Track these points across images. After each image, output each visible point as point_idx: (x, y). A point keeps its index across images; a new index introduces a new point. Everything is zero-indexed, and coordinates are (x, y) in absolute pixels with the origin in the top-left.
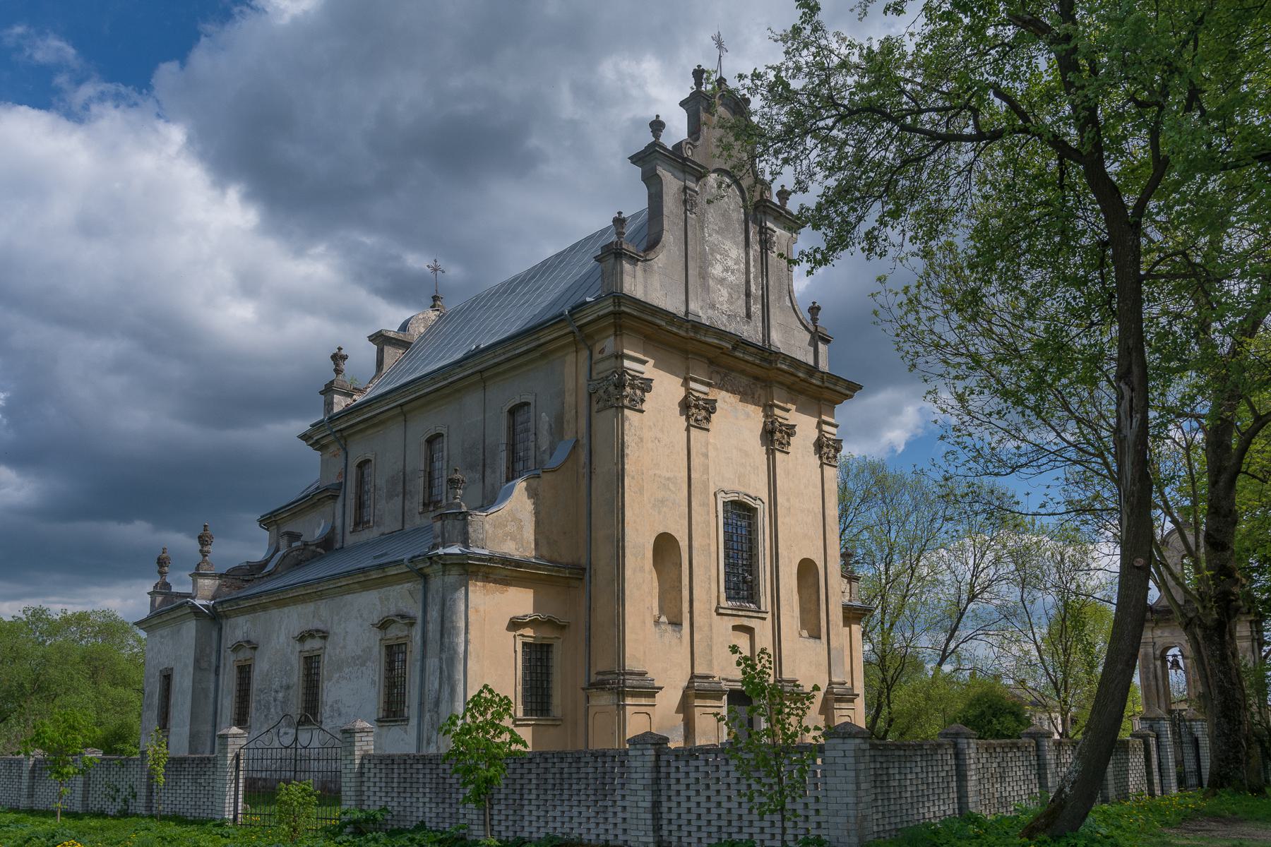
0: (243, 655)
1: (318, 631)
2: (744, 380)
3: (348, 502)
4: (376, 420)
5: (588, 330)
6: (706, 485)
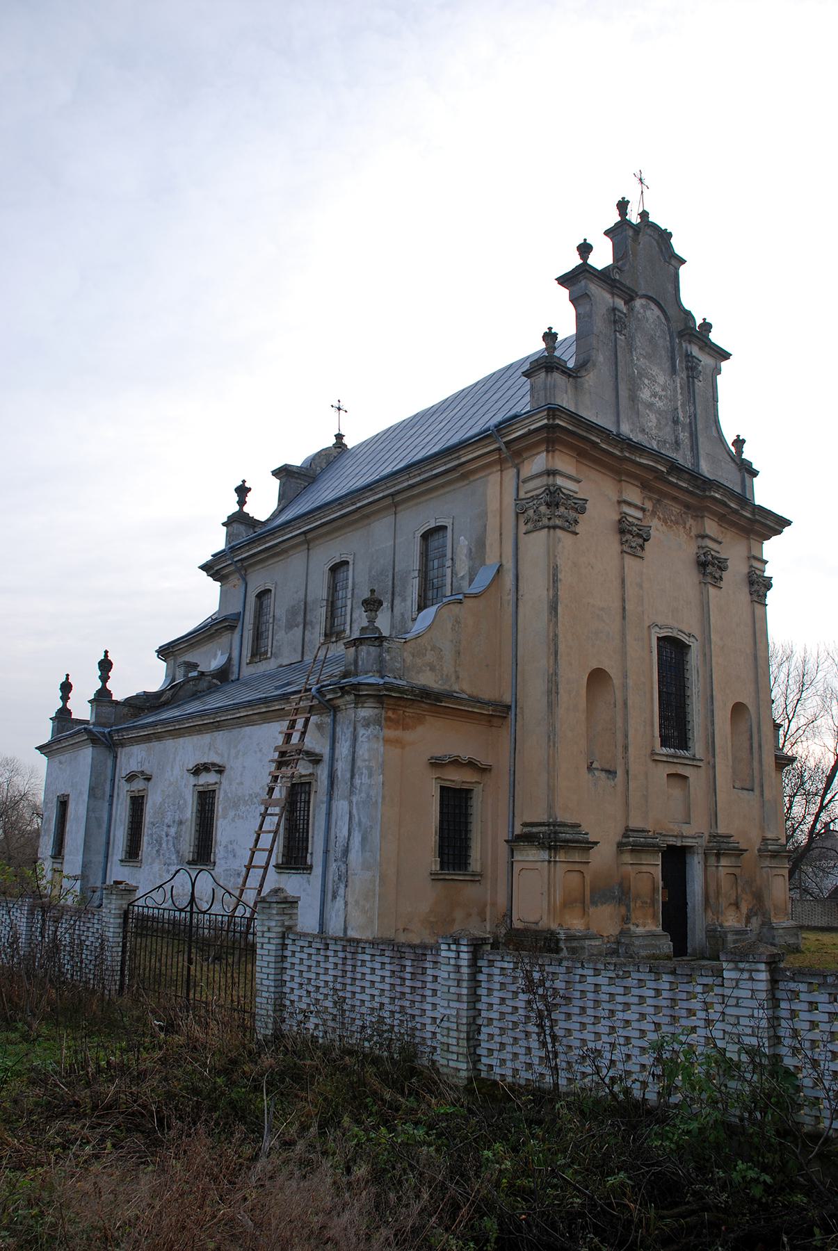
0: (138, 785)
1: (214, 765)
2: (676, 509)
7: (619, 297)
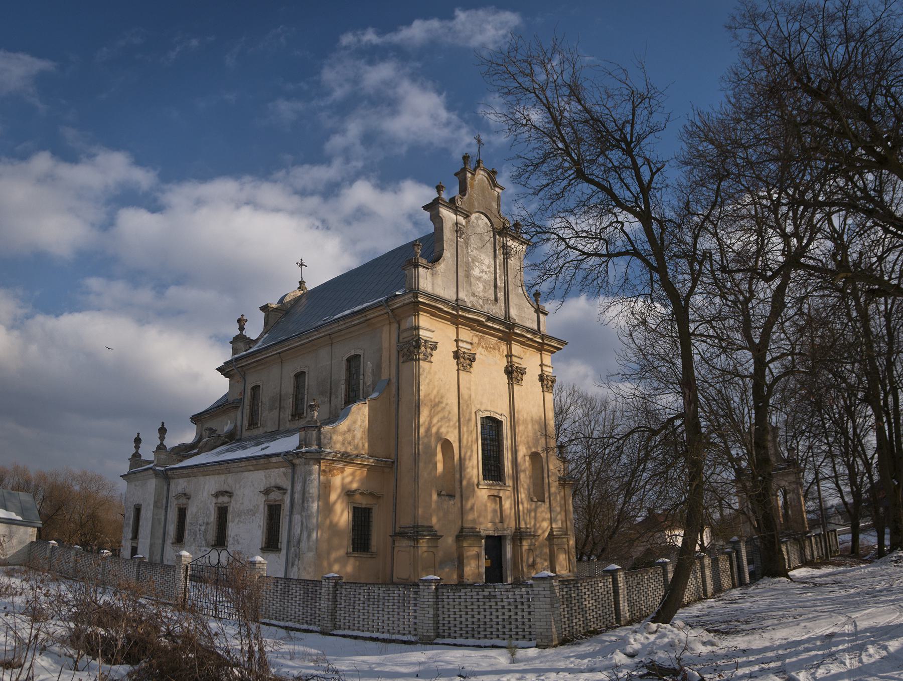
1: (227, 492)
4: (263, 361)
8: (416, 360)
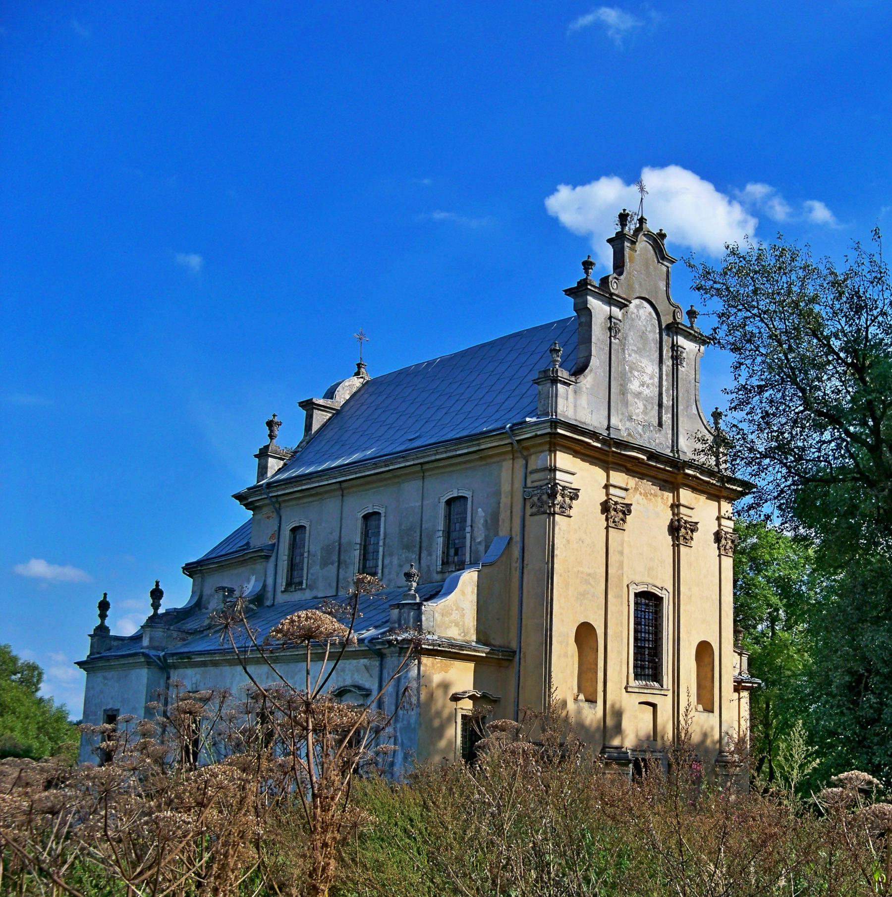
3: (280, 563)
5: (525, 444)
6: (620, 578)
7: (615, 306)
8: (550, 514)
